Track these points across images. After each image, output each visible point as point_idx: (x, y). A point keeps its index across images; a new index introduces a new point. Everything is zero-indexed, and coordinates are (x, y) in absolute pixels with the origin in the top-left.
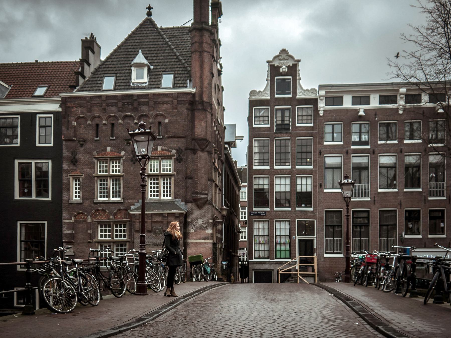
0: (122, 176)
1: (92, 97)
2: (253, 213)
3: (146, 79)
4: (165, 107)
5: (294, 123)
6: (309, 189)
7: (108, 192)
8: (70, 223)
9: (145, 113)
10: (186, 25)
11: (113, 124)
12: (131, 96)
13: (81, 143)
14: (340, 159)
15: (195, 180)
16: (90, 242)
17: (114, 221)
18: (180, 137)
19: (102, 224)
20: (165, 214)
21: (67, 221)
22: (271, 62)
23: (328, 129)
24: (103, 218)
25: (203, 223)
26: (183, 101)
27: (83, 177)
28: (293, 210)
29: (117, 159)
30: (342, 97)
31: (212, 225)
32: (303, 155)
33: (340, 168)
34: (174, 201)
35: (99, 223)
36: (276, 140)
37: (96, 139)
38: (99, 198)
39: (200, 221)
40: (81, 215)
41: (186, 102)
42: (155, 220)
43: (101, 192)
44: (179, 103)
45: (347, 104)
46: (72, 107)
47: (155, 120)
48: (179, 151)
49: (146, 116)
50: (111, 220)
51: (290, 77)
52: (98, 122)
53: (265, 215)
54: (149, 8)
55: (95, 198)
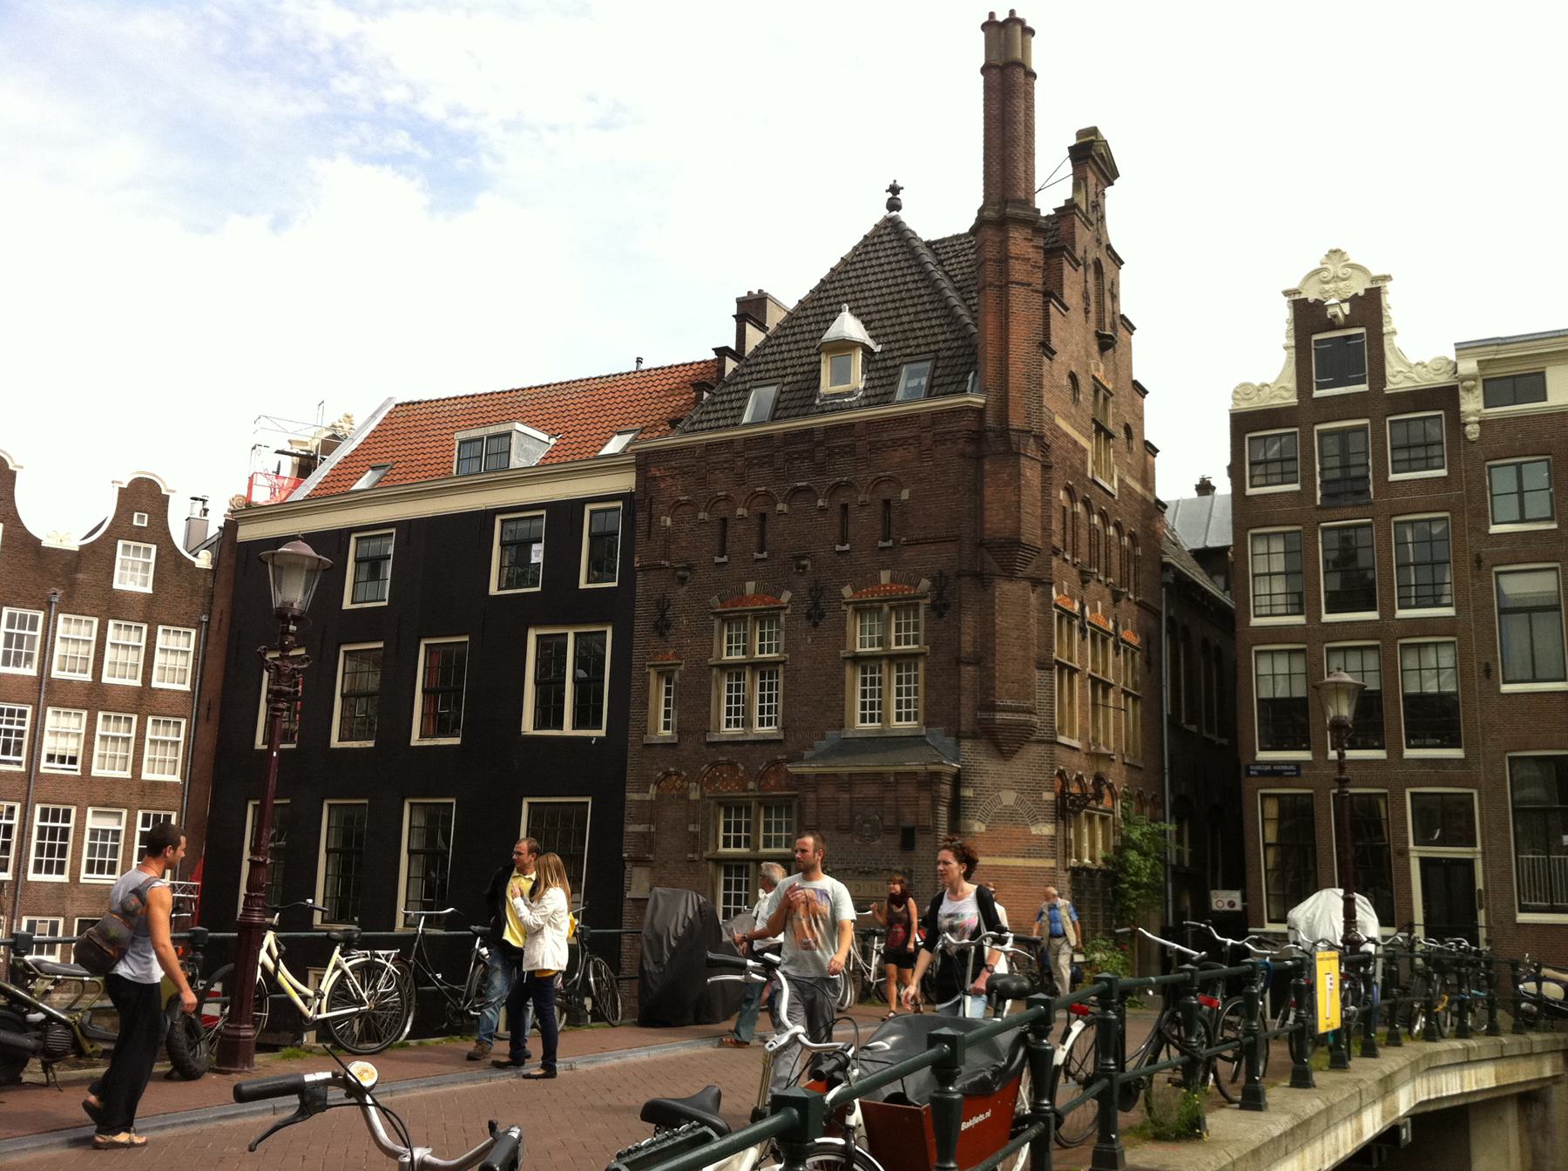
0: (783, 662)
1: (710, 447)
2: (1259, 768)
3: (858, 380)
4: (898, 456)
5: (1381, 473)
7: (747, 712)
8: (643, 802)
9: (845, 479)
11: (763, 516)
12: (808, 432)
13: (680, 573)
14: (1552, 577)
16: (692, 861)
17: (758, 797)
18: (944, 540)
19: (729, 806)
20: (888, 773)
21: (635, 797)
22: (1296, 292)
23: (1502, 480)
24: (731, 790)
25: (1019, 801)
26: (950, 432)
27: (682, 668)
29: (766, 617)
30: (1542, 375)
31: (1051, 810)
33: (1557, 608)
34: (924, 733)
35: (720, 804)
36: (1325, 530)
37: (718, 560)
38: (723, 728)
39: (1009, 798)
40: (675, 778)
41: (959, 435)
43: (729, 712)
46: (663, 478)
47: (874, 496)
48: (941, 583)
49: (849, 485)
50: (751, 794)
51: (1362, 330)
52: (726, 514)
53: (1298, 775)
54: (894, 189)
55: (712, 728)
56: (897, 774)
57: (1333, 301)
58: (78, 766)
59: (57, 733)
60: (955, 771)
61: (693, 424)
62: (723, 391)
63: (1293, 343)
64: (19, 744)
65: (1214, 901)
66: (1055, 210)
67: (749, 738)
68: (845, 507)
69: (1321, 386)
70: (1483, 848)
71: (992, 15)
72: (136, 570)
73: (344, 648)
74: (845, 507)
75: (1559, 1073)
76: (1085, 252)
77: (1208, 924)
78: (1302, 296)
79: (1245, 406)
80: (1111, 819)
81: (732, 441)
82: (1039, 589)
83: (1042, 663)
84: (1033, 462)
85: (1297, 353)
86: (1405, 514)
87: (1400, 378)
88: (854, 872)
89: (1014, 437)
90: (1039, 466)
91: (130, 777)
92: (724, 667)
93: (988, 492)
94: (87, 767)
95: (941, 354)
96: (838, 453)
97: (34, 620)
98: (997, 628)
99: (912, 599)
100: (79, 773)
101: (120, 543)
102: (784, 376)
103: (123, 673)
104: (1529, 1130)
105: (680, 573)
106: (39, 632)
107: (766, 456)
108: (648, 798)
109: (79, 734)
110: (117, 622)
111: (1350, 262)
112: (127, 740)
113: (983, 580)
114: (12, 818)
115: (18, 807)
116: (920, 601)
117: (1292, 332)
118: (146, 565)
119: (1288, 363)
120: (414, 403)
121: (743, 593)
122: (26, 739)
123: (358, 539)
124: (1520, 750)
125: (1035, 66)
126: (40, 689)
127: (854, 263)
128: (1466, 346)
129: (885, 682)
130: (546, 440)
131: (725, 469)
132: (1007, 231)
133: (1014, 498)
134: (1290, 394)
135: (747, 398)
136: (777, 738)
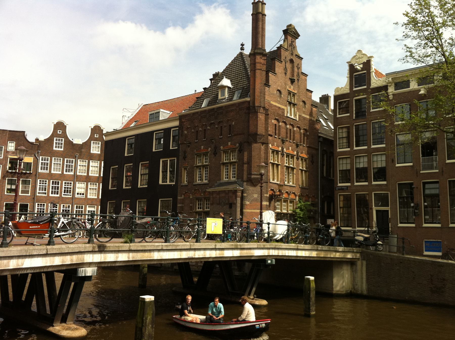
2: (338, 188)
3: (227, 95)
6: (384, 165)
10: (271, 50)
11: (205, 130)
12: (213, 109)
13: (188, 145)
19: (199, 199)
29: (205, 154)
34: (236, 181)
35: (197, 199)
41: (245, 108)
45: (414, 85)
46: (185, 122)
48: (241, 144)
49: (222, 122)
50: (202, 196)
53: (347, 189)
54: (242, 45)
56: (228, 191)
57: (356, 64)
58: (84, 196)
59: (79, 188)
61: (192, 108)
63: (349, 76)
64: (70, 191)
65: (328, 222)
66: (277, 48)
67: (202, 183)
68: (221, 127)
69: (355, 87)
70: (390, 207)
72: (96, 148)
73: (125, 165)
76: (286, 58)
78: (351, 63)
79: (337, 94)
81: (198, 112)
82: (264, 145)
84: (262, 114)
86: (375, 120)
87: (374, 84)
89: (256, 108)
91: (97, 198)
92: (197, 167)
93: (251, 122)
94: (86, 196)
97: (72, 161)
100: (85, 197)
101: (92, 142)
103: (85, 172)
104: (353, 271)
105: (188, 145)
106: (74, 164)
108: (182, 198)
109: (84, 188)
110: (92, 161)
111: (363, 53)
112: (96, 189)
114: (69, 208)
115: (70, 205)
117: (349, 73)
118: (99, 147)
119: (348, 80)
120: (147, 105)
121: (201, 149)
122: (72, 189)
123: (128, 139)
124: (400, 181)
127: (231, 65)
128: (404, 71)
133: (256, 123)
134: (348, 90)
135: (203, 101)
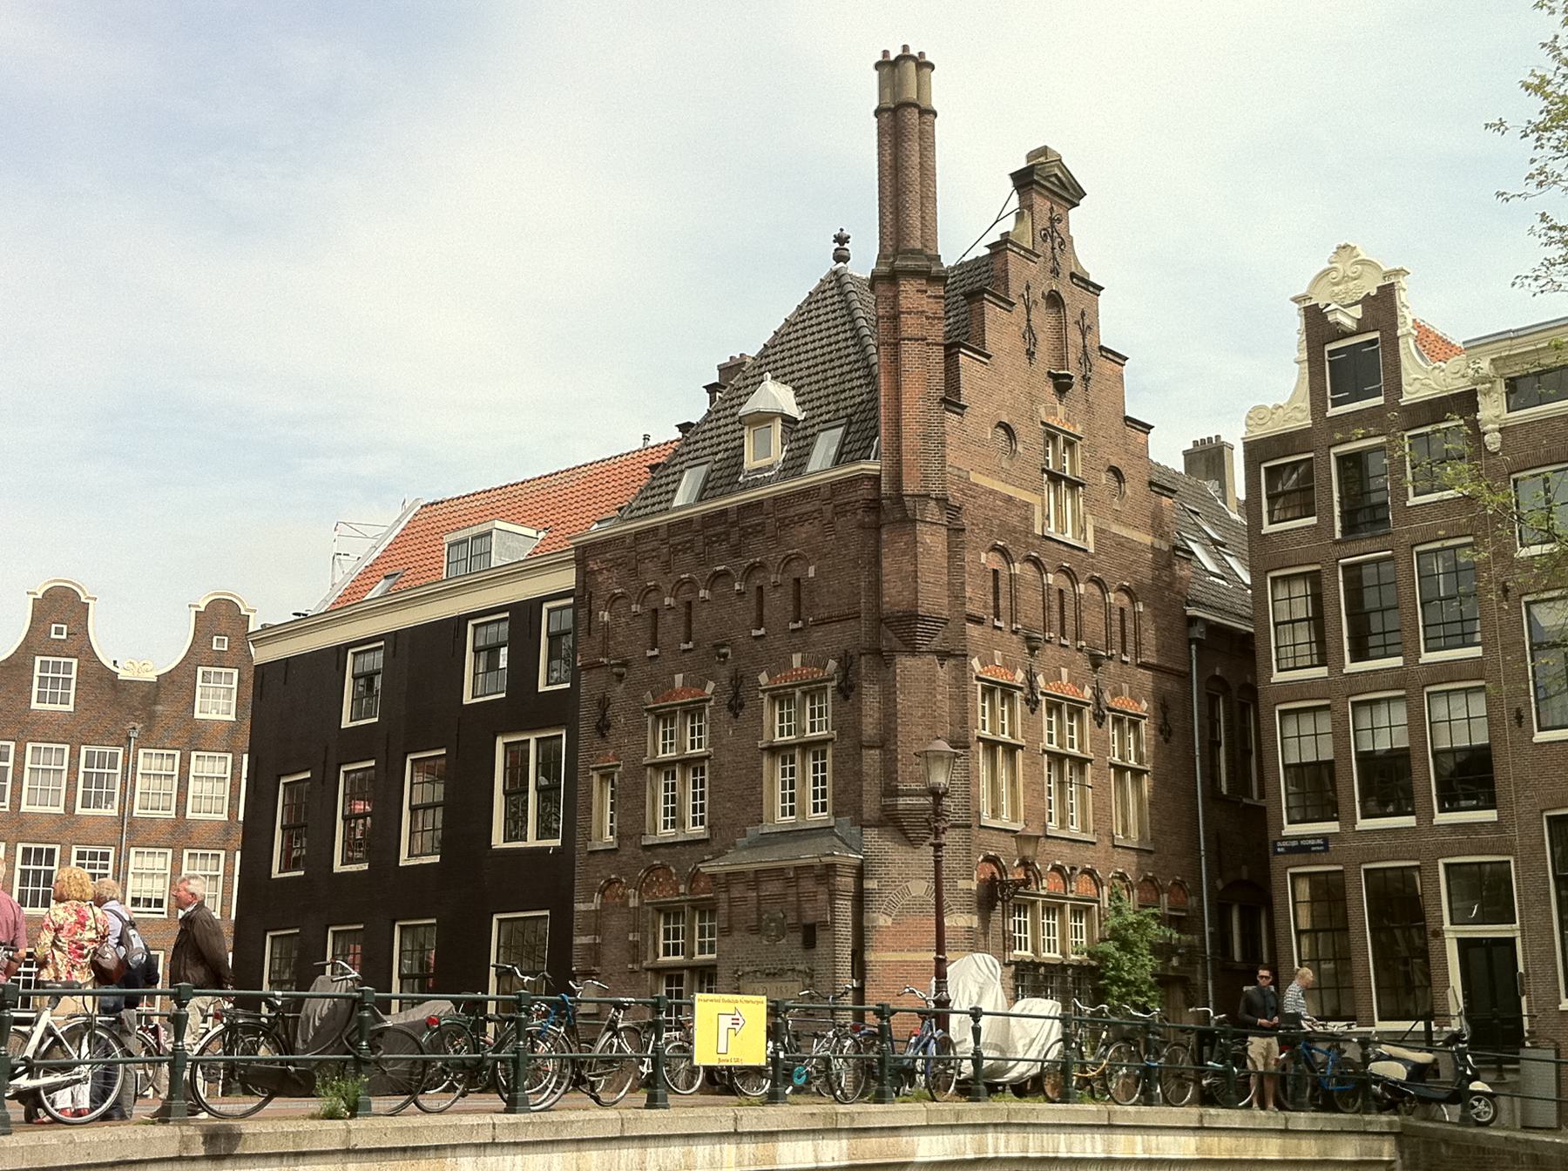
0: (708, 757)
2: (1285, 844)
4: (804, 531)
10: (966, 259)
13: (615, 670)
15: (890, 751)
16: (633, 972)
17: (689, 900)
19: (670, 912)
20: (788, 868)
22: (1306, 298)
24: (664, 895)
26: (848, 503)
27: (621, 769)
28: (1425, 826)
29: (694, 711)
32: (1385, 616)
35: (659, 911)
42: (766, 891)
44: (840, 511)
46: (600, 571)
47: (786, 575)
48: (847, 664)
50: (683, 898)
52: (656, 605)
53: (1327, 849)
54: (841, 240)
56: (796, 868)
60: (859, 862)
61: (632, 511)
62: (662, 474)
63: (1305, 356)
67: (679, 840)
68: (760, 588)
69: (1336, 403)
71: (886, 53)
74: (760, 588)
75: (1393, 1158)
76: (1028, 288)
77: (514, 965)
79: (1260, 433)
80: (1096, 909)
81: (657, 528)
83: (956, 742)
85: (1310, 367)
87: (1417, 385)
88: (762, 974)
89: (908, 502)
90: (944, 531)
92: (658, 766)
95: (854, 419)
96: (751, 534)
98: (899, 707)
99: (821, 682)
102: (716, 453)
105: (615, 670)
107: (687, 542)
113: (883, 659)
116: (828, 684)
121: (673, 687)
123: (355, 654)
125: (936, 104)
126: (122, 831)
129: (798, 771)
130: (534, 535)
131: (653, 557)
132: (896, 284)
136: (701, 837)
